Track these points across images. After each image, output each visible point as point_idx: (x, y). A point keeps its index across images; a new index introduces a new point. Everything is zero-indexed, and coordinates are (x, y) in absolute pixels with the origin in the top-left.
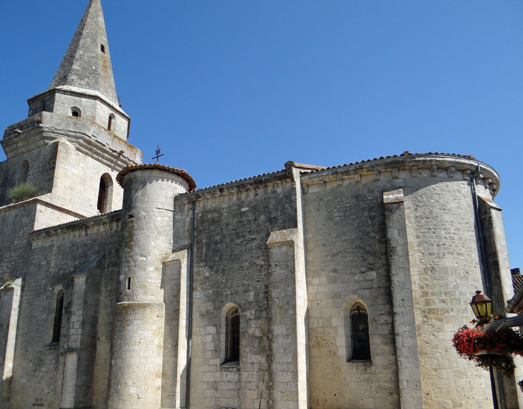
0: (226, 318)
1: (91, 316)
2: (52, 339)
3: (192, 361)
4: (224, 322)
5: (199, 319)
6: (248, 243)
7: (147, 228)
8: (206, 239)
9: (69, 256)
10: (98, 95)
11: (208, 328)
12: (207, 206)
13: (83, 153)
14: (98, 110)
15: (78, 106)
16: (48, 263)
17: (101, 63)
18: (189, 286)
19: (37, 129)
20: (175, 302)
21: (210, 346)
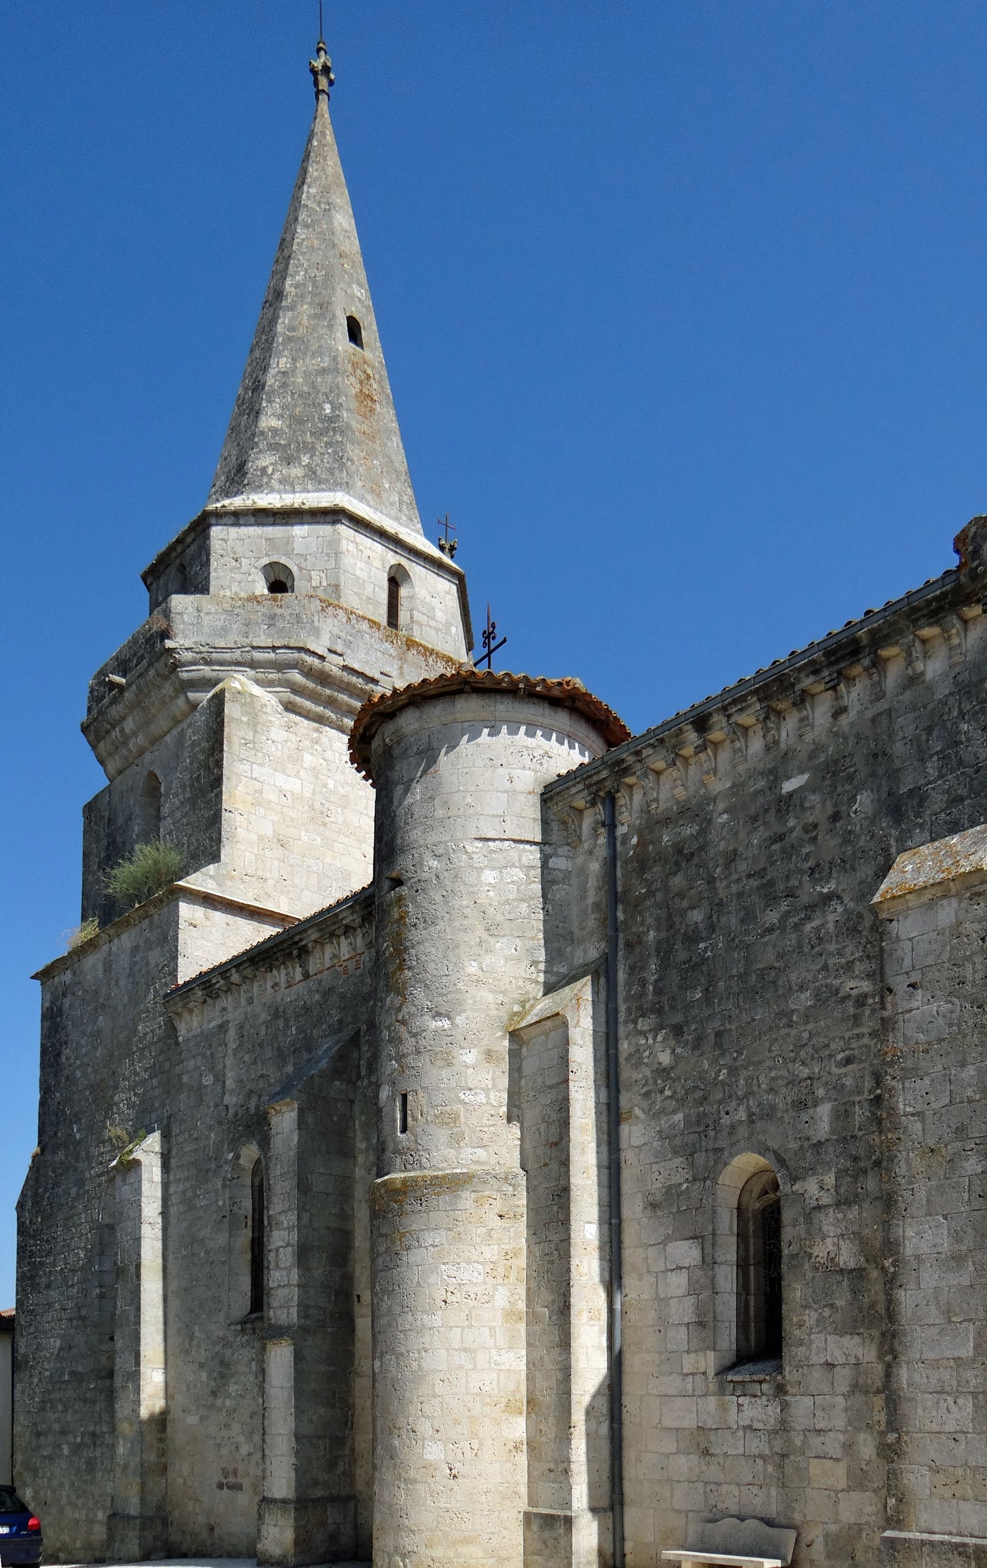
0: (738, 1209)
1: (328, 1228)
2: (249, 1302)
3: (627, 1361)
4: (731, 1221)
5: (645, 1220)
6: (808, 918)
7: (447, 916)
8: (658, 930)
9: (268, 1053)
10: (340, 505)
11: (673, 1248)
12: (656, 800)
13: (307, 717)
14: (347, 561)
15: (283, 560)
16: (220, 1079)
17: (351, 385)
18: (604, 1109)
19: (163, 659)
20: (554, 1166)
21: (683, 1311)
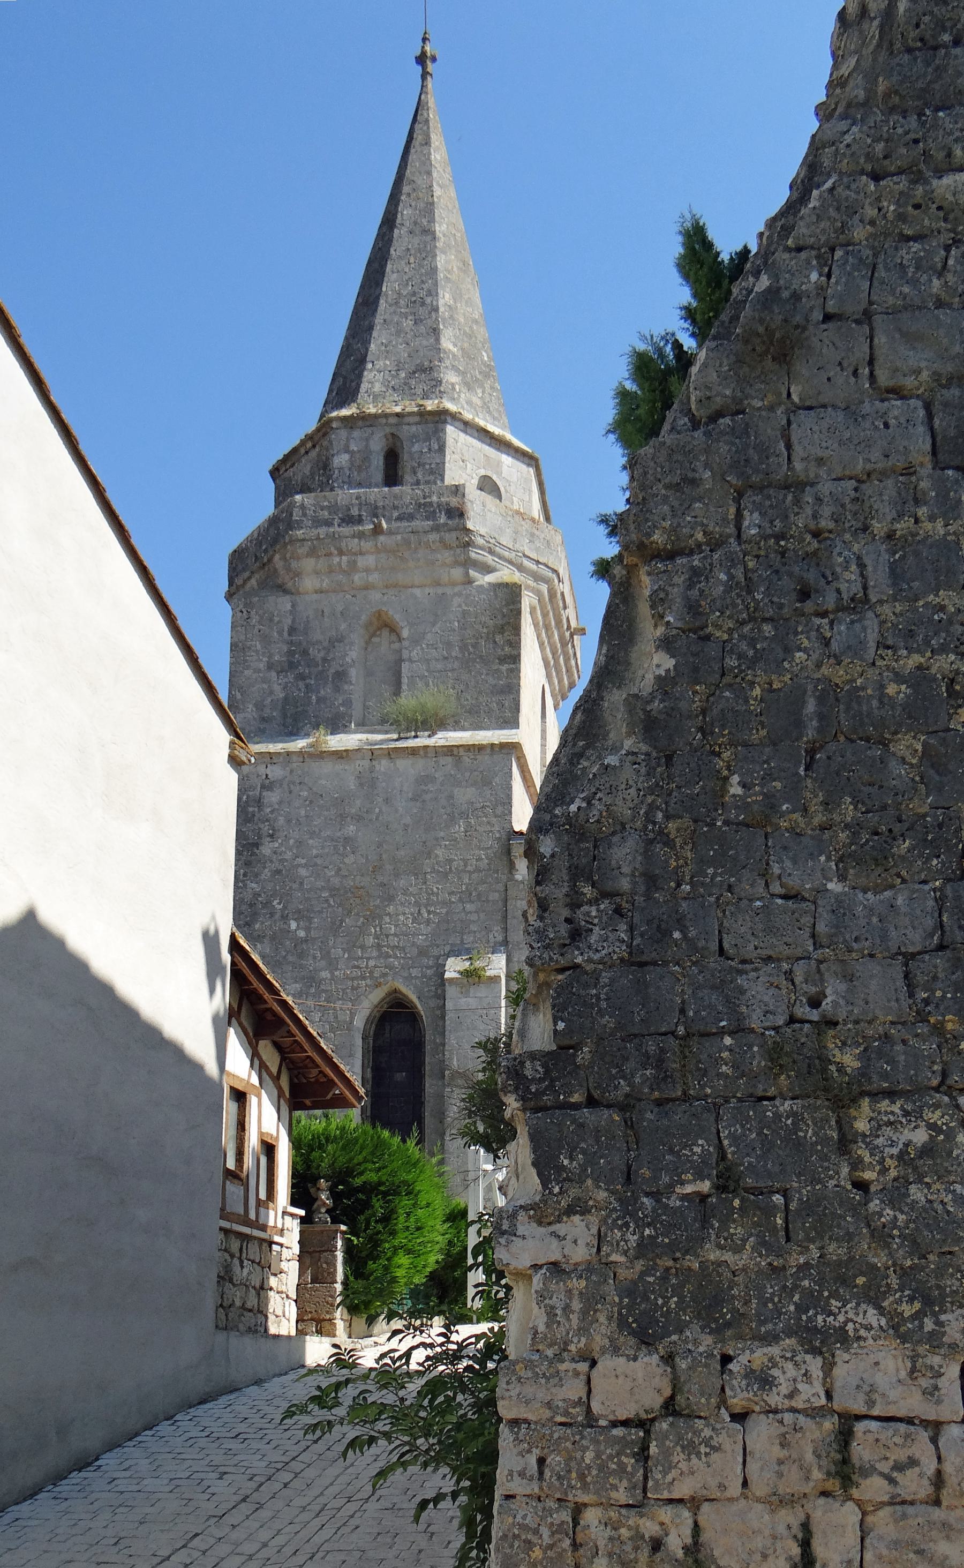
15: (494, 478)
